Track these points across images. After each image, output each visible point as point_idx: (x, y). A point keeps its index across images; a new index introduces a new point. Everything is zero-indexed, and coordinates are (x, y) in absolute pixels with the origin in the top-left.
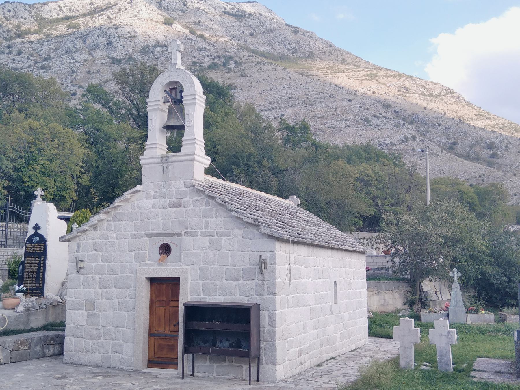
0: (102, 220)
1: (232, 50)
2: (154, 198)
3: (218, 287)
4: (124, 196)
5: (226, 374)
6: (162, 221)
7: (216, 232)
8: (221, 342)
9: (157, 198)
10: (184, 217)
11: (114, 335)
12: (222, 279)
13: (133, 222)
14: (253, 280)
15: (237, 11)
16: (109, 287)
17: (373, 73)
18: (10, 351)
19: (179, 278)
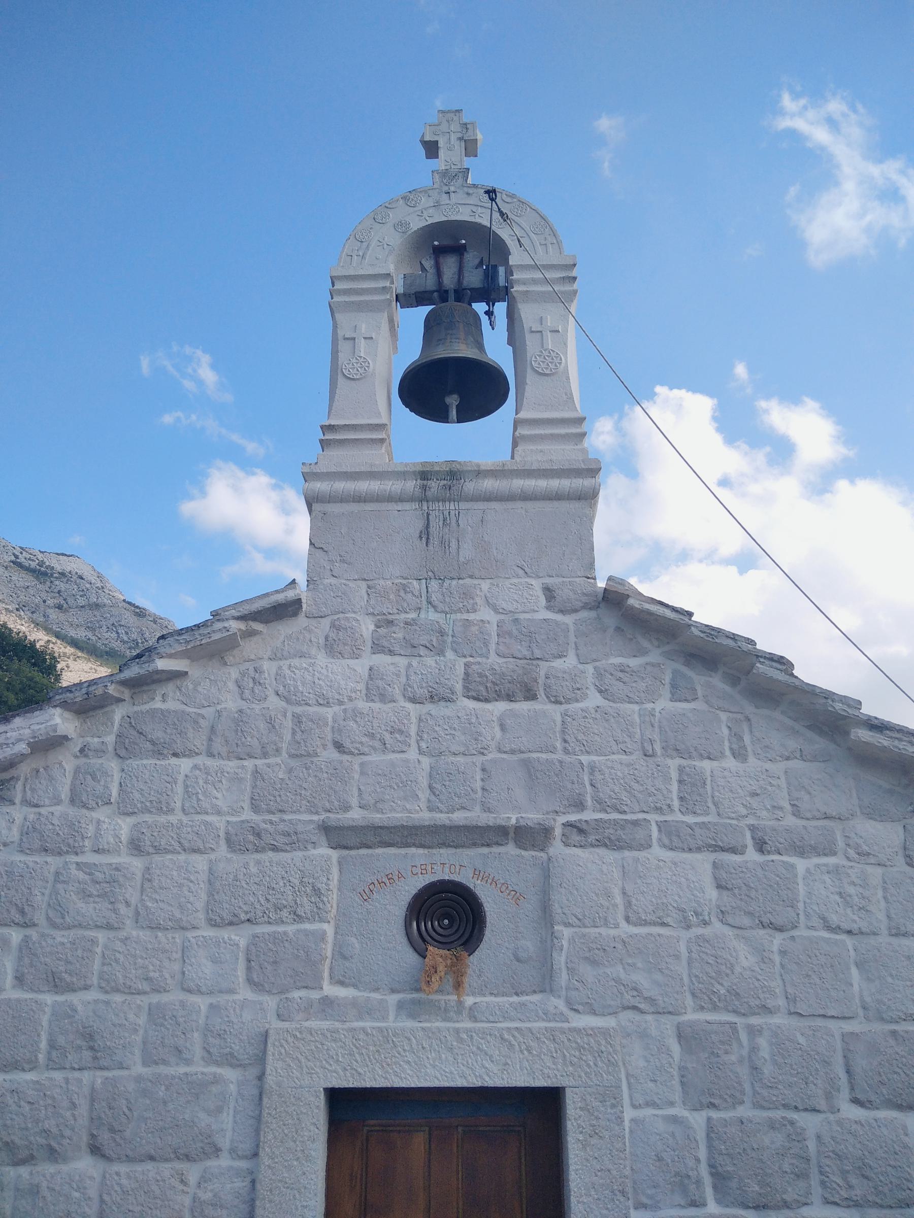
0: (56, 742)
2: (378, 648)
3: (812, 1145)
6: (426, 761)
7: (753, 828)
9: (391, 653)
10: (559, 745)
12: (829, 1096)
13: (249, 764)
15: (38, 565)
16: (53, 1155)
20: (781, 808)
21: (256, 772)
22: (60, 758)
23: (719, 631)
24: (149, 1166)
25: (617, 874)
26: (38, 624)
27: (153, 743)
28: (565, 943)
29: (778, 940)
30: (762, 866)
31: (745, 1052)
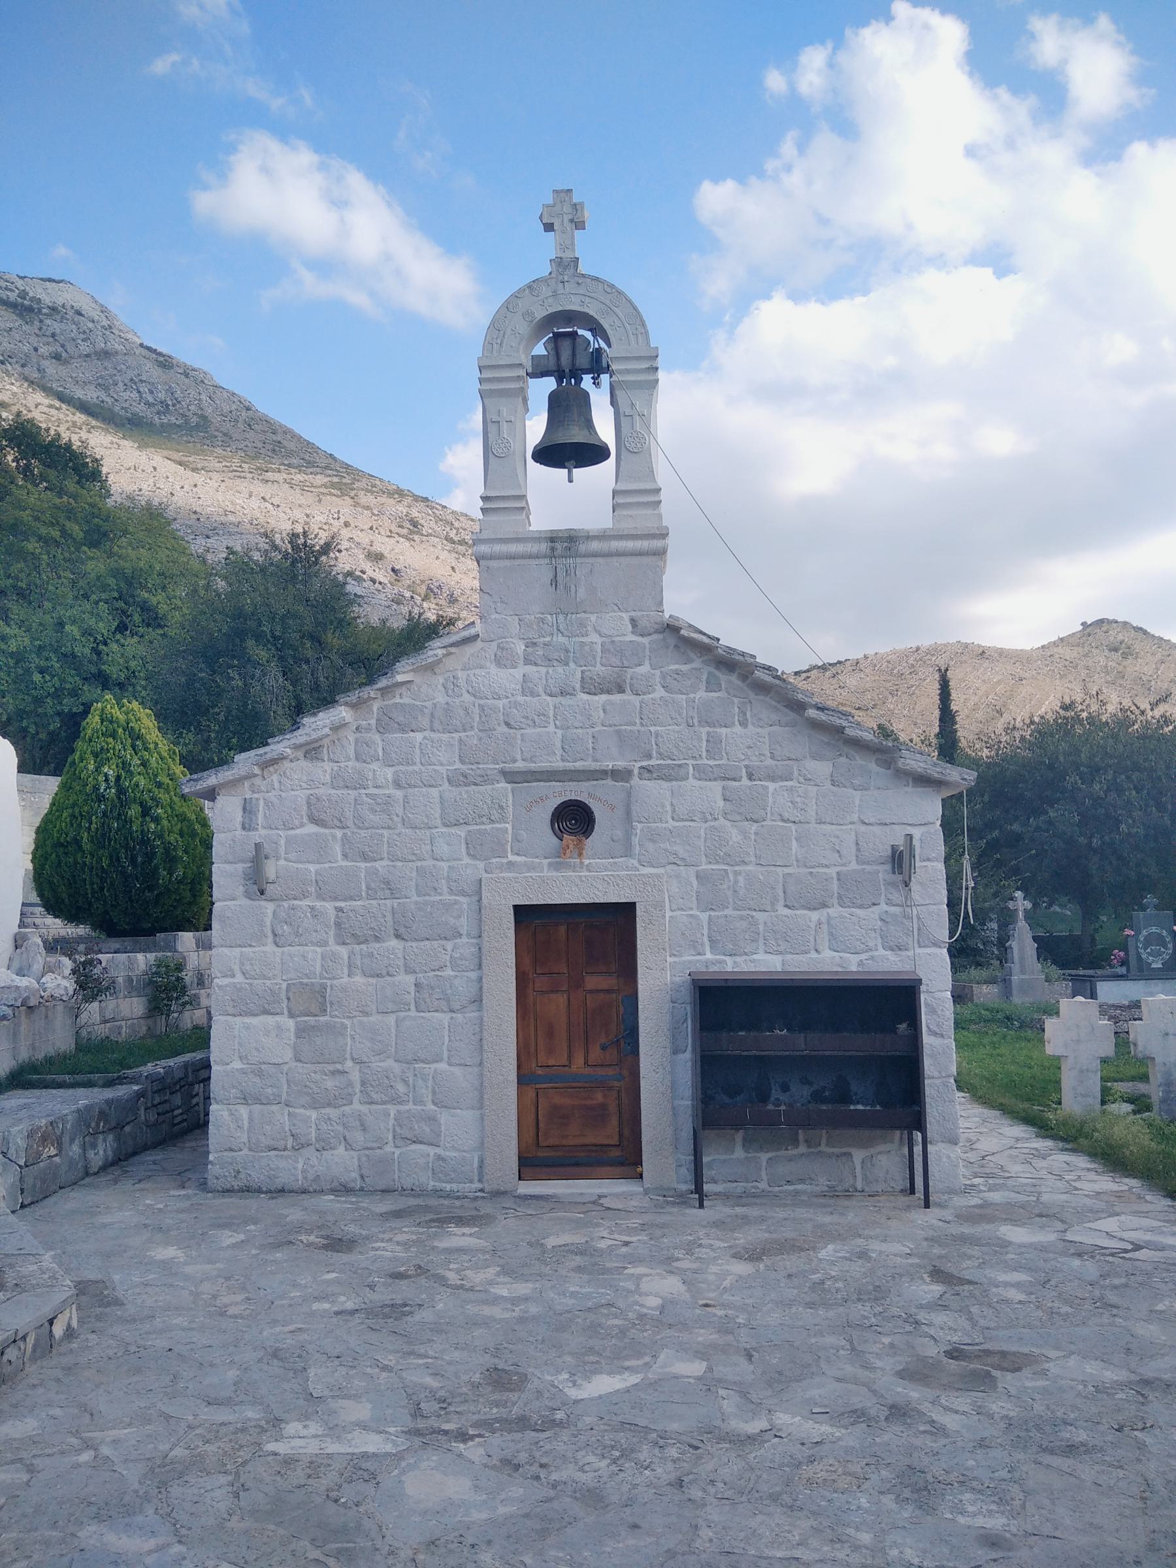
1: (8, 387)
2: (527, 661)
3: (761, 927)
4: (431, 653)
5: (802, 1181)
6: (560, 733)
7: (747, 767)
8: (785, 1088)
9: (536, 664)
11: (401, 1088)
12: (772, 904)
14: (874, 904)
16: (377, 939)
17: (344, 481)
18: (20, 1167)
19: (634, 904)
20: (764, 755)
21: (460, 740)
22: (345, 733)
23: (734, 650)
24: (427, 942)
25: (668, 794)
26: (32, 382)
27: (398, 723)
28: (638, 831)
29: (755, 826)
30: (750, 788)
31: (731, 884)
